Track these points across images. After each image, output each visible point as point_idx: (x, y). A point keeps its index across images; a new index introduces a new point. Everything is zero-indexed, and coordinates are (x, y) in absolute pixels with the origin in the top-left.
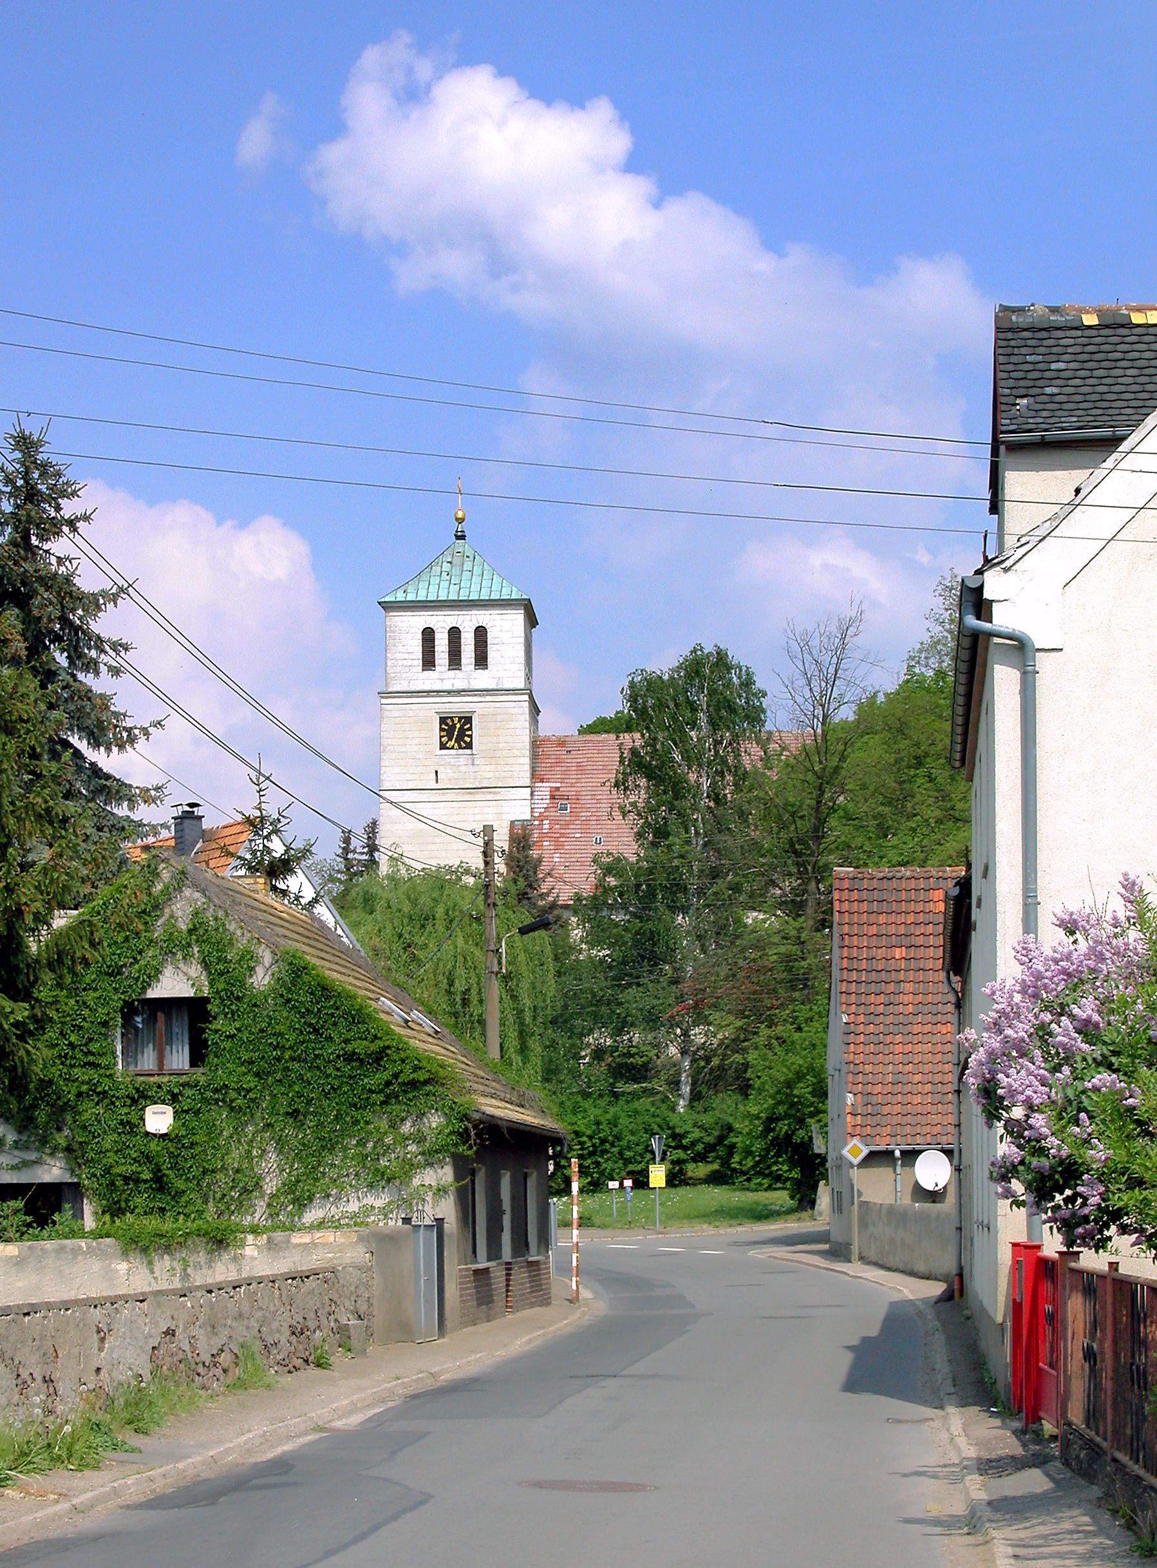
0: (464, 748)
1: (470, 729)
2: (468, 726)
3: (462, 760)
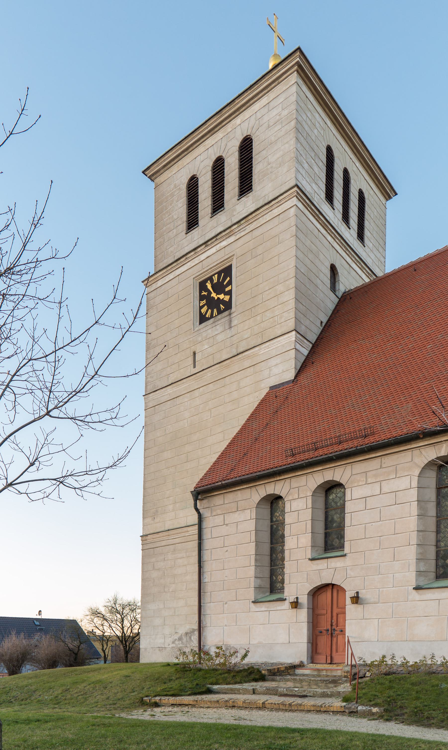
0: (225, 310)
1: (230, 283)
2: (228, 279)
3: (219, 328)
